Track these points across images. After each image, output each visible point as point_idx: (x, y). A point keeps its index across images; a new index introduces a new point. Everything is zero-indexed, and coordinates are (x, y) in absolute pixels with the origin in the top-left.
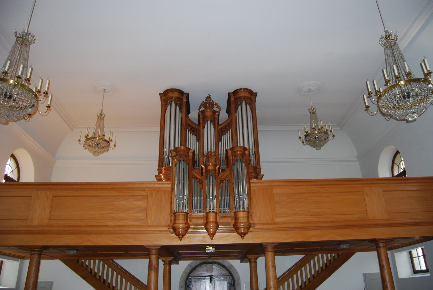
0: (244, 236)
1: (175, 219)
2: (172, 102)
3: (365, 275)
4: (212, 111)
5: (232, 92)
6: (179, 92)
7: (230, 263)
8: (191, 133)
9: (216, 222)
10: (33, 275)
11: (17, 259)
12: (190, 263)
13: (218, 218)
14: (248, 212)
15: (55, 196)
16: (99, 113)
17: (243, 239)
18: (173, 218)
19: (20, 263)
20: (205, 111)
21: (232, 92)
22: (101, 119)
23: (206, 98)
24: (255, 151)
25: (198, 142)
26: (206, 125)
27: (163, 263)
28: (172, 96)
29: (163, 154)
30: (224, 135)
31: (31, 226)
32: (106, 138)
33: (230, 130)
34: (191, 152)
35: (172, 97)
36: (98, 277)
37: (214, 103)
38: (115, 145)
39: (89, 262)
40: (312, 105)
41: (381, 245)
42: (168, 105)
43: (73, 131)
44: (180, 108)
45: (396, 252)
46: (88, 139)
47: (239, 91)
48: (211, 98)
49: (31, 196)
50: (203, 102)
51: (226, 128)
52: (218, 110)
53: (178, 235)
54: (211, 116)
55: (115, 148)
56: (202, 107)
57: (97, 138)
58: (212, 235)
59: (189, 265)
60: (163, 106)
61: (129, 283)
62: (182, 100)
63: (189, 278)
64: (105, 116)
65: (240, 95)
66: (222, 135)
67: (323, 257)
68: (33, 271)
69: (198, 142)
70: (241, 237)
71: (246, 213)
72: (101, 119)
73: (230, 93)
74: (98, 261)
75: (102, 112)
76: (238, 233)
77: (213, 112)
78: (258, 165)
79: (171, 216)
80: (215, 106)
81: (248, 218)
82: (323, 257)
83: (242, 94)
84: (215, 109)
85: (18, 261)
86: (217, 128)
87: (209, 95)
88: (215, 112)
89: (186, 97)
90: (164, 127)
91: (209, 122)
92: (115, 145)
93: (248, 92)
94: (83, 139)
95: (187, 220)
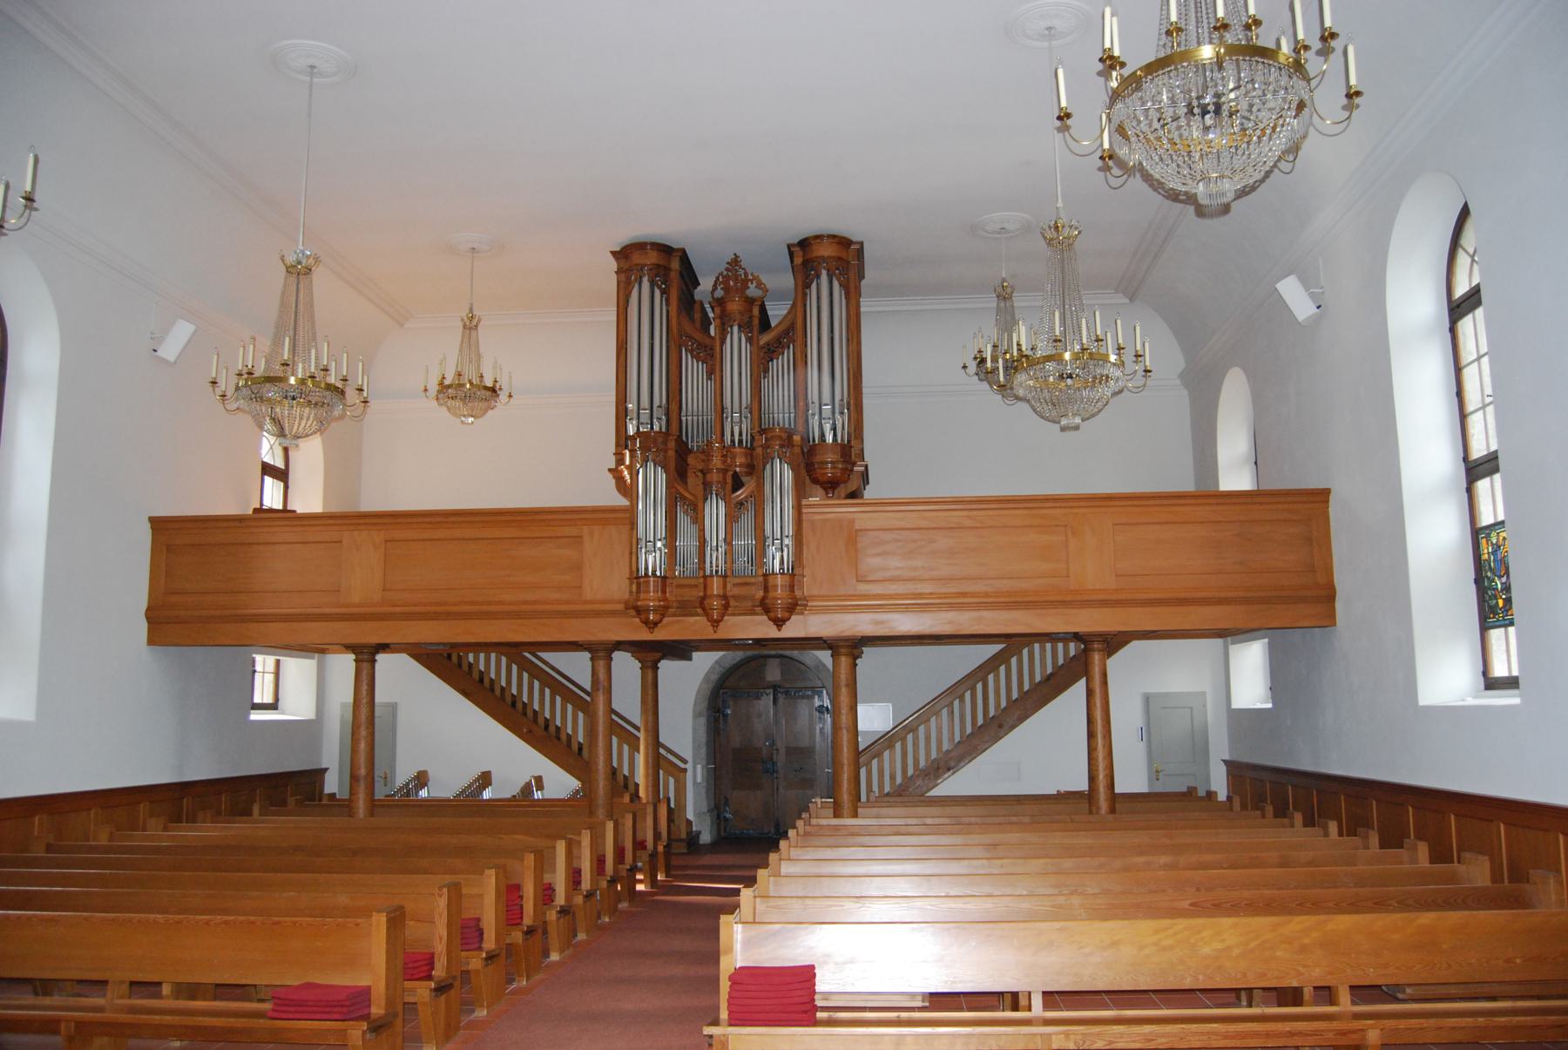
0: (782, 625)
1: (638, 592)
2: (641, 278)
3: (1148, 698)
4: (743, 299)
5: (796, 242)
6: (658, 250)
7: (817, 658)
8: (692, 357)
9: (725, 597)
10: (364, 701)
11: (311, 654)
12: (721, 658)
13: (729, 586)
14: (793, 575)
15: (389, 541)
16: (464, 313)
17: (779, 630)
18: (634, 587)
19: (318, 662)
20: (726, 300)
21: (796, 241)
22: (470, 329)
23: (728, 263)
24: (848, 403)
25: (711, 380)
26: (729, 336)
27: (640, 665)
28: (642, 262)
29: (626, 416)
30: (775, 361)
31: (348, 606)
32: (489, 384)
33: (791, 346)
34: (671, 440)
35: (642, 267)
36: (498, 692)
37: (750, 277)
38: (510, 393)
39: (474, 657)
40: (1004, 276)
41: (1096, 646)
42: (633, 287)
43: (405, 326)
44: (663, 292)
45: (1233, 643)
46: (443, 387)
47: (813, 242)
48: (741, 263)
49: (340, 542)
50: (719, 274)
51: (780, 343)
52: (758, 293)
53: (646, 622)
54: (741, 313)
55: (511, 400)
56: (719, 288)
57: (466, 384)
58: (715, 623)
59: (716, 662)
60: (622, 285)
61: (570, 707)
62: (667, 269)
63: (721, 691)
64: (479, 321)
65: (815, 254)
66: (768, 362)
67: (1043, 650)
68: (364, 692)
69: (711, 380)
70: (775, 627)
71: (787, 578)
72: (470, 329)
73: (793, 245)
74: (496, 657)
75: (471, 310)
76: (770, 619)
77: (745, 301)
78: (856, 438)
79: (631, 584)
80: (752, 283)
81: (792, 587)
82: (1043, 650)
83: (826, 250)
84: (752, 291)
85: (313, 658)
86: (758, 340)
87: (735, 254)
88: (750, 301)
89: (678, 258)
90: (626, 343)
91: (736, 329)
92: (510, 393)
93: (837, 243)
94: (434, 388)
95: (664, 592)
